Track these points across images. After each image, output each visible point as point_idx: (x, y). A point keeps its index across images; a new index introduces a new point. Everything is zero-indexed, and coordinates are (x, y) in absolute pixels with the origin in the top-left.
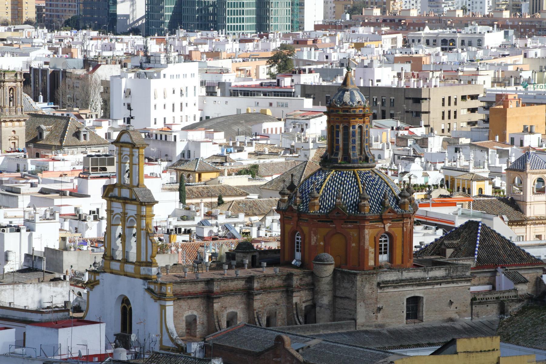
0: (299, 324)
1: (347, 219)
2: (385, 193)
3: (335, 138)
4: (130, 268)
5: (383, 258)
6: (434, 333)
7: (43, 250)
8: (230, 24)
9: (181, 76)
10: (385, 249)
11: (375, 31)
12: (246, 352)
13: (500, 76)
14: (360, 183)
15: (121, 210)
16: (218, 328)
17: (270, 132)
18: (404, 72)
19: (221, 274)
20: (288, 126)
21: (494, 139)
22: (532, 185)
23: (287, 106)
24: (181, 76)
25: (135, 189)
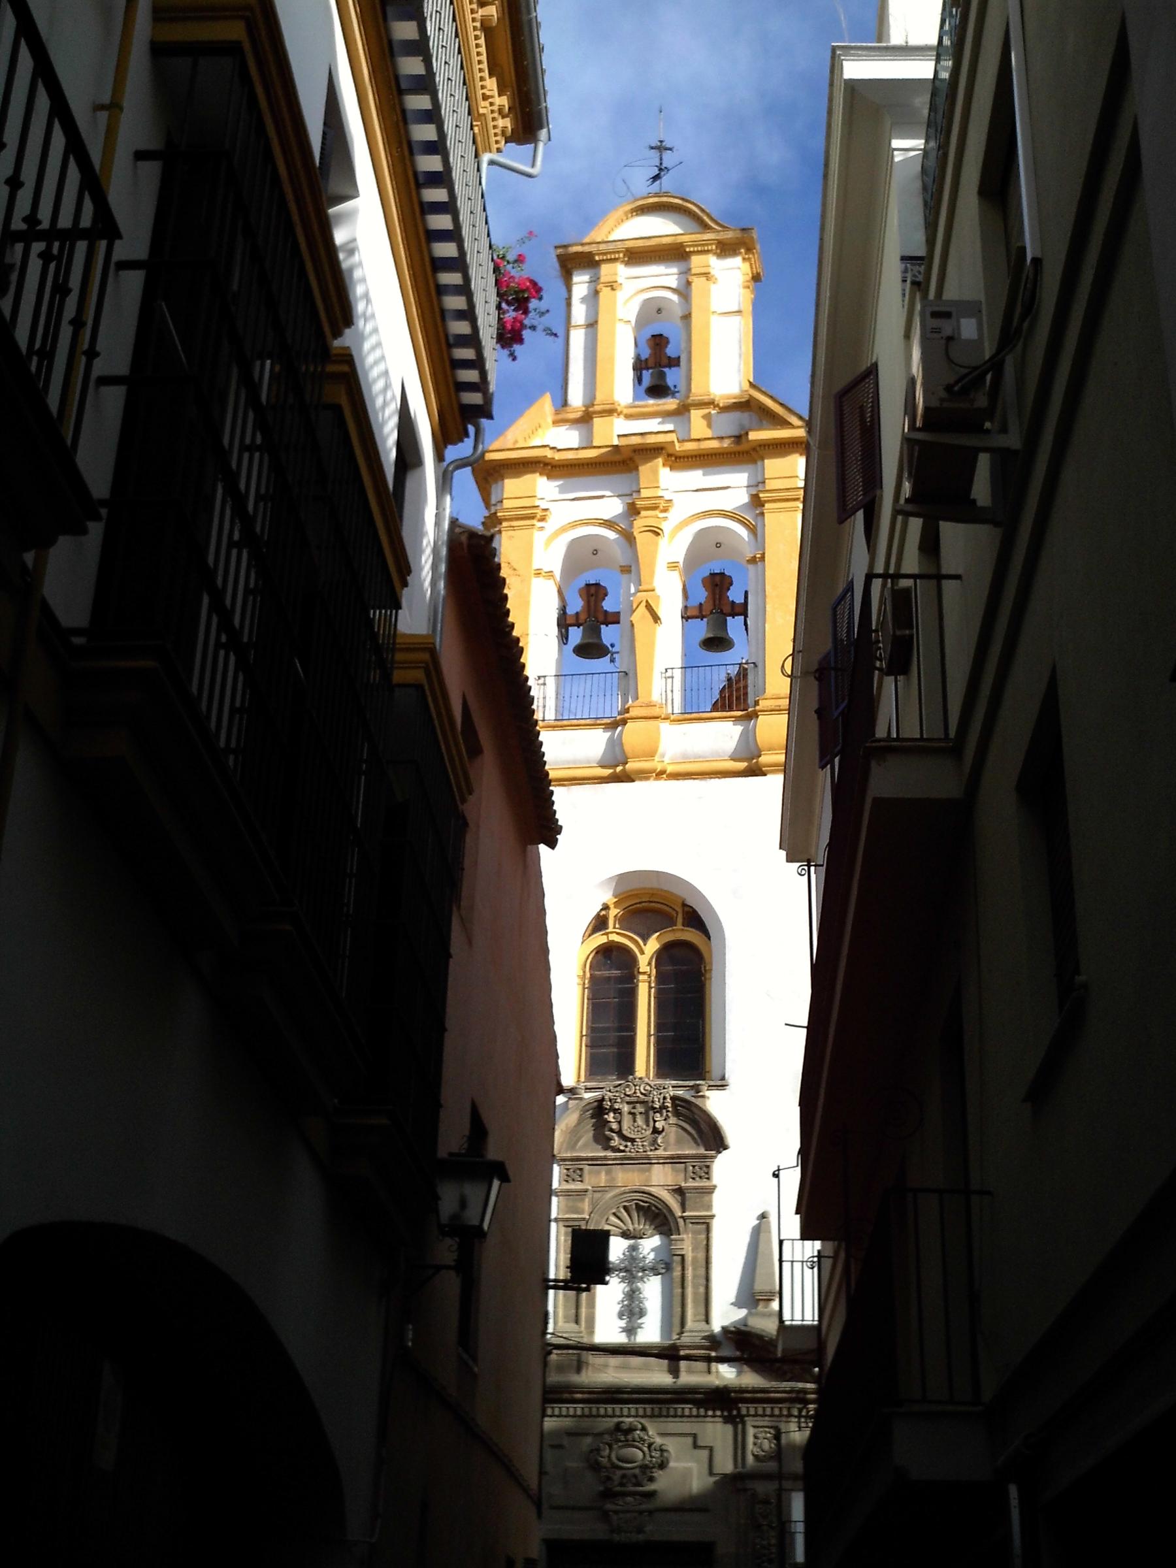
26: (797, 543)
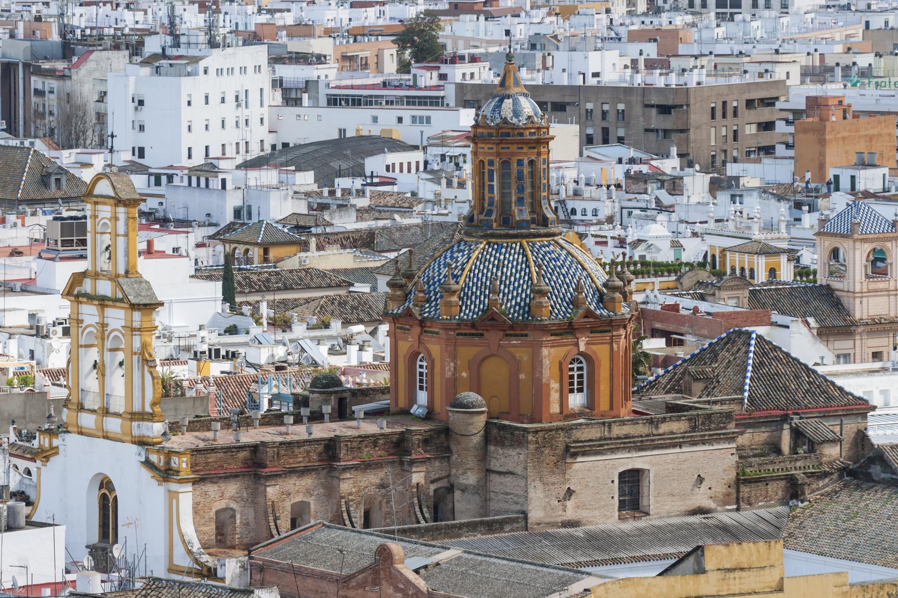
0: (423, 522)
1: (510, 330)
3: (487, 183)
4: (113, 425)
5: (576, 400)
9: (237, 71)
10: (580, 383)
12: (323, 576)
13: (818, 64)
14: (532, 264)
15: (97, 319)
16: (274, 532)
18: (643, 57)
19: (281, 434)
22: (864, 262)
24: (237, 71)
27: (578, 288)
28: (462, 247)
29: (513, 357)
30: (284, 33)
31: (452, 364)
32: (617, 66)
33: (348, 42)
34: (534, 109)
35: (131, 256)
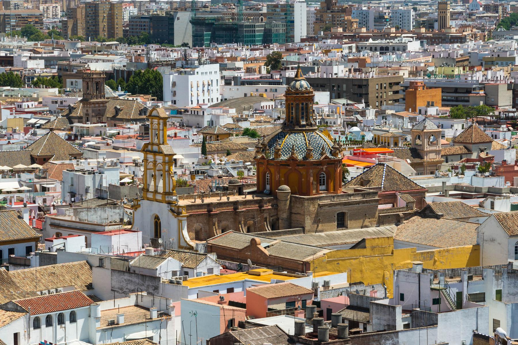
2: (323, 146)
3: (291, 111)
6: (354, 235)
7: (108, 186)
8: (246, 39)
9: (208, 73)
11: (338, 42)
14: (307, 140)
17: (265, 108)
18: (353, 68)
20: (277, 104)
21: (408, 111)
23: (276, 90)
24: (208, 73)
25: (161, 146)
26: (295, 256)
27: (323, 149)
28: (282, 134)
29: (300, 172)
30: (226, 60)
31: (278, 175)
32: (343, 71)
33: (249, 63)
34: (307, 85)
35: (165, 137)
